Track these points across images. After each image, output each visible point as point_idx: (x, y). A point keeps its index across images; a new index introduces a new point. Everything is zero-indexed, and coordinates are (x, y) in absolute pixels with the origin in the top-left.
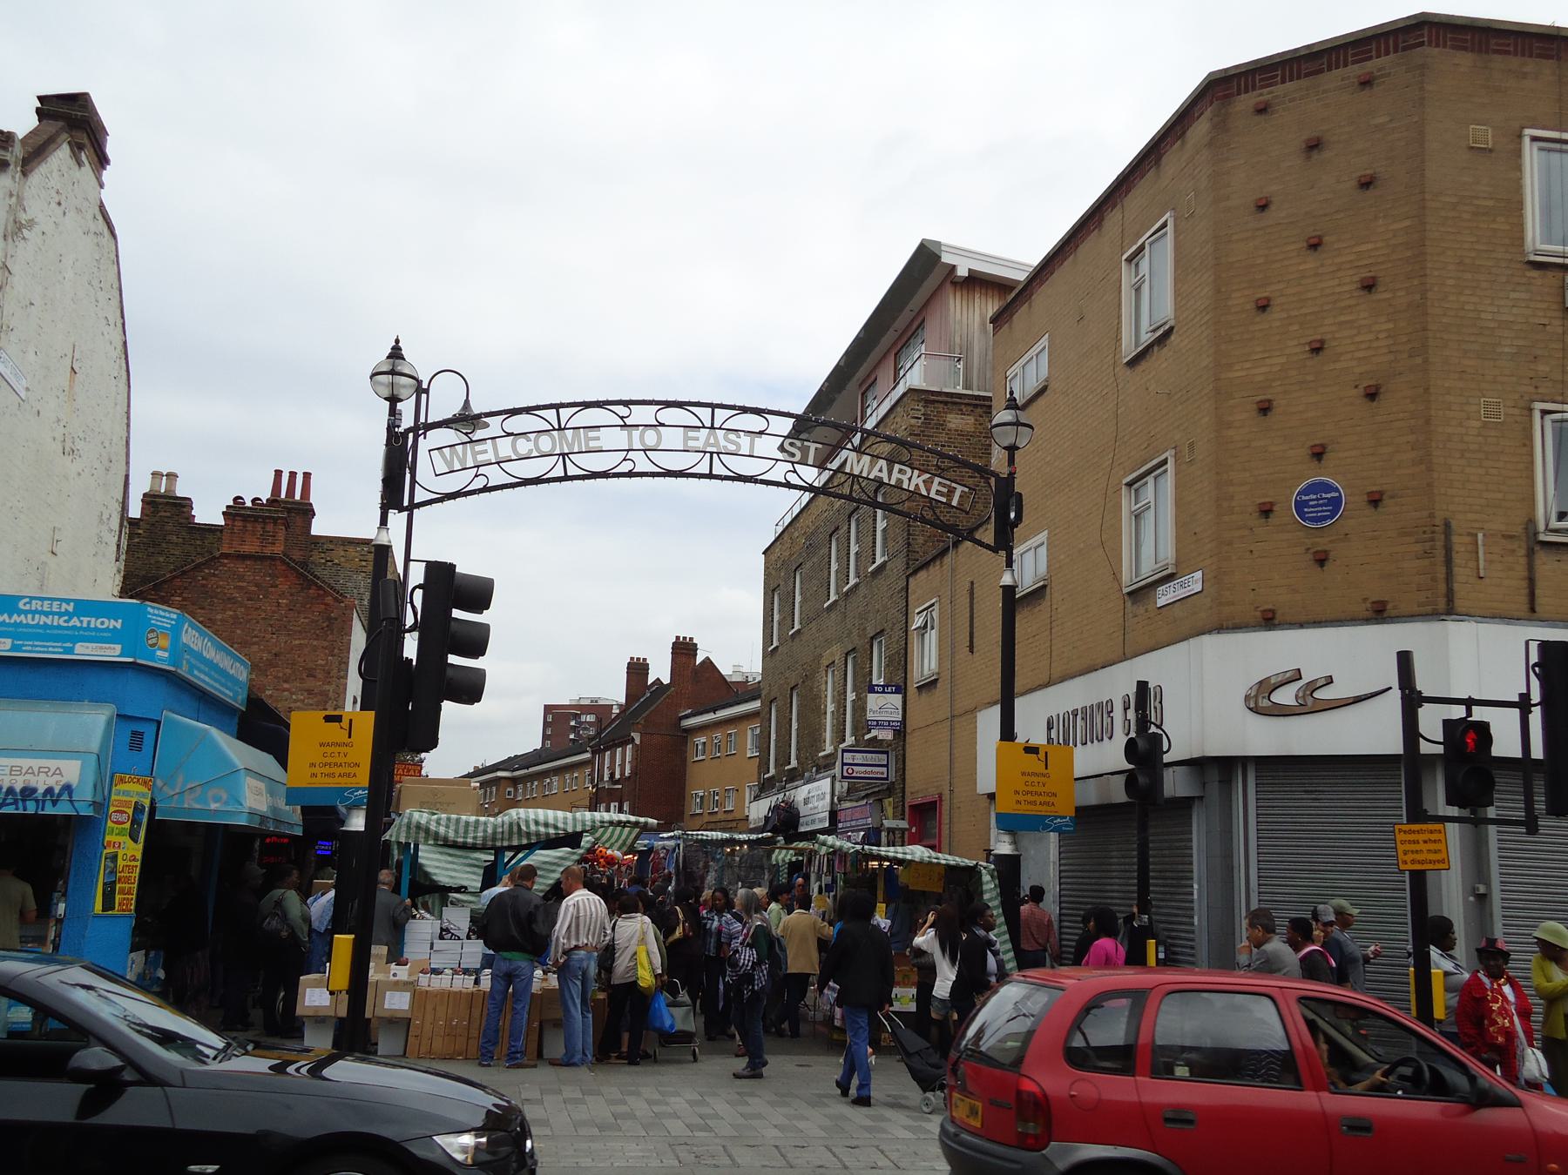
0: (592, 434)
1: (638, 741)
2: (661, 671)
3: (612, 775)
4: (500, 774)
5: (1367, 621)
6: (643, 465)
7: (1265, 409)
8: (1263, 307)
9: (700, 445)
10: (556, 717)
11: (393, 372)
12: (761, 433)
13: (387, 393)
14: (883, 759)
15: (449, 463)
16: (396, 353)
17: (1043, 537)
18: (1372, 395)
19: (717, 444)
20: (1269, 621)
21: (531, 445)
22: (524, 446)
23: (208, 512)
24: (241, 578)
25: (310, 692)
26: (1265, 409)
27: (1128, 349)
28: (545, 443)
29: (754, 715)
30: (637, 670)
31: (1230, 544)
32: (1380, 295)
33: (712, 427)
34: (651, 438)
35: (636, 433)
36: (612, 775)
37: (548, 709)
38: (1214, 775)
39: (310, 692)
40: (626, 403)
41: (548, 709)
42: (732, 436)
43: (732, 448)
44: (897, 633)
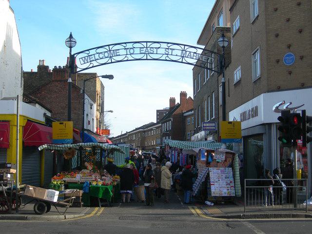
0: (117, 51)
1: (172, 120)
2: (178, 101)
3: (167, 129)
4: (141, 130)
5: (300, 88)
6: (130, 58)
7: (277, 36)
8: (276, 10)
9: (144, 52)
10: (159, 113)
11: (70, 41)
12: (159, 48)
13: (69, 45)
14: (214, 124)
15: (84, 61)
16: (71, 36)
17: (240, 68)
18: (300, 31)
19: (148, 51)
20: (279, 89)
21: (103, 55)
22: (101, 56)
23: (51, 68)
24: (57, 86)
25: (75, 113)
26: (277, 36)
27: (252, 19)
28: (106, 55)
29: (192, 114)
30: (172, 101)
31: (270, 70)
32: (302, 7)
33: (147, 47)
34: (132, 51)
35: (128, 50)
36: (167, 129)
37: (158, 111)
38: (267, 126)
39: (75, 113)
40: (125, 43)
41: (158, 111)
42: (152, 49)
43: (152, 52)
44: (216, 92)
